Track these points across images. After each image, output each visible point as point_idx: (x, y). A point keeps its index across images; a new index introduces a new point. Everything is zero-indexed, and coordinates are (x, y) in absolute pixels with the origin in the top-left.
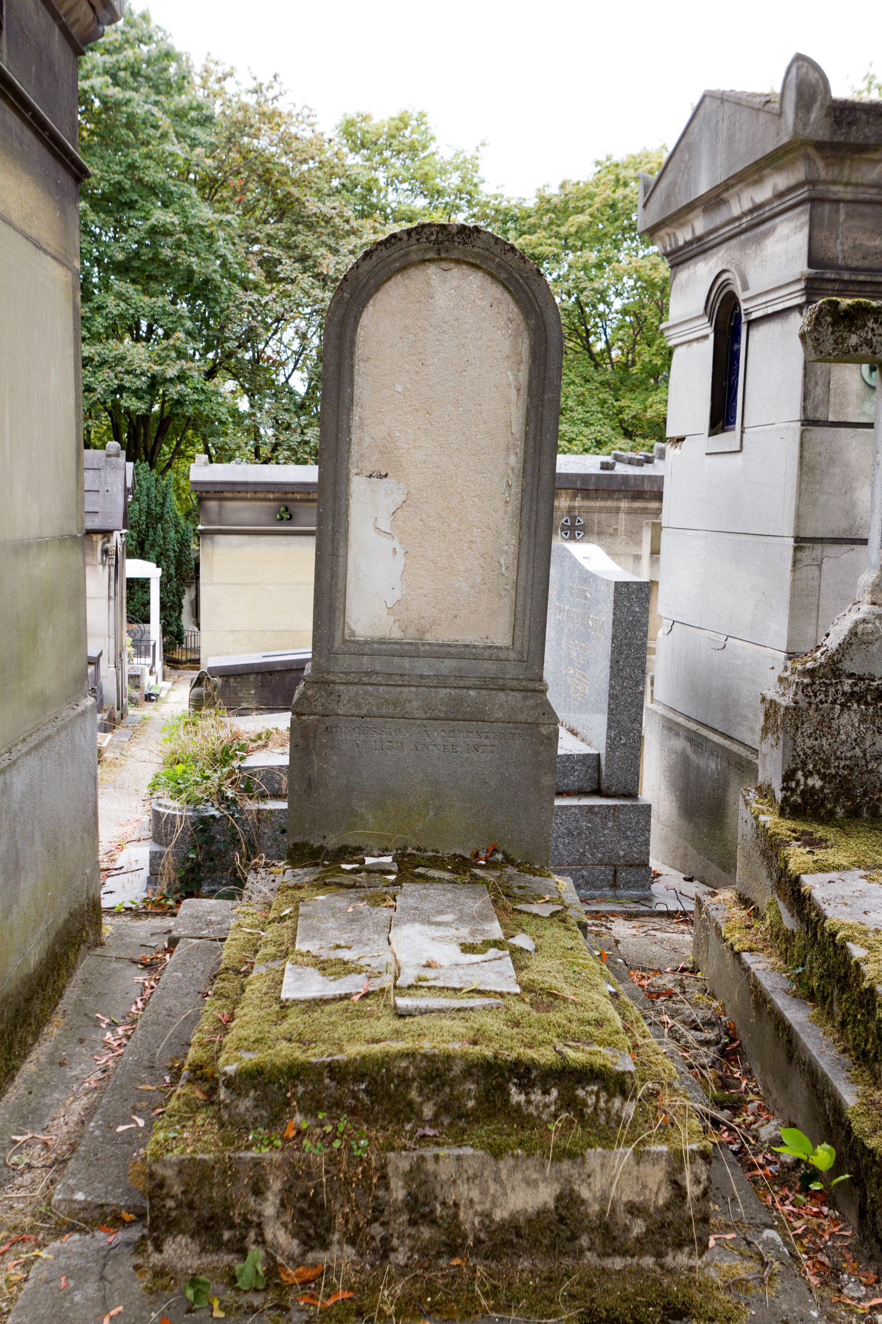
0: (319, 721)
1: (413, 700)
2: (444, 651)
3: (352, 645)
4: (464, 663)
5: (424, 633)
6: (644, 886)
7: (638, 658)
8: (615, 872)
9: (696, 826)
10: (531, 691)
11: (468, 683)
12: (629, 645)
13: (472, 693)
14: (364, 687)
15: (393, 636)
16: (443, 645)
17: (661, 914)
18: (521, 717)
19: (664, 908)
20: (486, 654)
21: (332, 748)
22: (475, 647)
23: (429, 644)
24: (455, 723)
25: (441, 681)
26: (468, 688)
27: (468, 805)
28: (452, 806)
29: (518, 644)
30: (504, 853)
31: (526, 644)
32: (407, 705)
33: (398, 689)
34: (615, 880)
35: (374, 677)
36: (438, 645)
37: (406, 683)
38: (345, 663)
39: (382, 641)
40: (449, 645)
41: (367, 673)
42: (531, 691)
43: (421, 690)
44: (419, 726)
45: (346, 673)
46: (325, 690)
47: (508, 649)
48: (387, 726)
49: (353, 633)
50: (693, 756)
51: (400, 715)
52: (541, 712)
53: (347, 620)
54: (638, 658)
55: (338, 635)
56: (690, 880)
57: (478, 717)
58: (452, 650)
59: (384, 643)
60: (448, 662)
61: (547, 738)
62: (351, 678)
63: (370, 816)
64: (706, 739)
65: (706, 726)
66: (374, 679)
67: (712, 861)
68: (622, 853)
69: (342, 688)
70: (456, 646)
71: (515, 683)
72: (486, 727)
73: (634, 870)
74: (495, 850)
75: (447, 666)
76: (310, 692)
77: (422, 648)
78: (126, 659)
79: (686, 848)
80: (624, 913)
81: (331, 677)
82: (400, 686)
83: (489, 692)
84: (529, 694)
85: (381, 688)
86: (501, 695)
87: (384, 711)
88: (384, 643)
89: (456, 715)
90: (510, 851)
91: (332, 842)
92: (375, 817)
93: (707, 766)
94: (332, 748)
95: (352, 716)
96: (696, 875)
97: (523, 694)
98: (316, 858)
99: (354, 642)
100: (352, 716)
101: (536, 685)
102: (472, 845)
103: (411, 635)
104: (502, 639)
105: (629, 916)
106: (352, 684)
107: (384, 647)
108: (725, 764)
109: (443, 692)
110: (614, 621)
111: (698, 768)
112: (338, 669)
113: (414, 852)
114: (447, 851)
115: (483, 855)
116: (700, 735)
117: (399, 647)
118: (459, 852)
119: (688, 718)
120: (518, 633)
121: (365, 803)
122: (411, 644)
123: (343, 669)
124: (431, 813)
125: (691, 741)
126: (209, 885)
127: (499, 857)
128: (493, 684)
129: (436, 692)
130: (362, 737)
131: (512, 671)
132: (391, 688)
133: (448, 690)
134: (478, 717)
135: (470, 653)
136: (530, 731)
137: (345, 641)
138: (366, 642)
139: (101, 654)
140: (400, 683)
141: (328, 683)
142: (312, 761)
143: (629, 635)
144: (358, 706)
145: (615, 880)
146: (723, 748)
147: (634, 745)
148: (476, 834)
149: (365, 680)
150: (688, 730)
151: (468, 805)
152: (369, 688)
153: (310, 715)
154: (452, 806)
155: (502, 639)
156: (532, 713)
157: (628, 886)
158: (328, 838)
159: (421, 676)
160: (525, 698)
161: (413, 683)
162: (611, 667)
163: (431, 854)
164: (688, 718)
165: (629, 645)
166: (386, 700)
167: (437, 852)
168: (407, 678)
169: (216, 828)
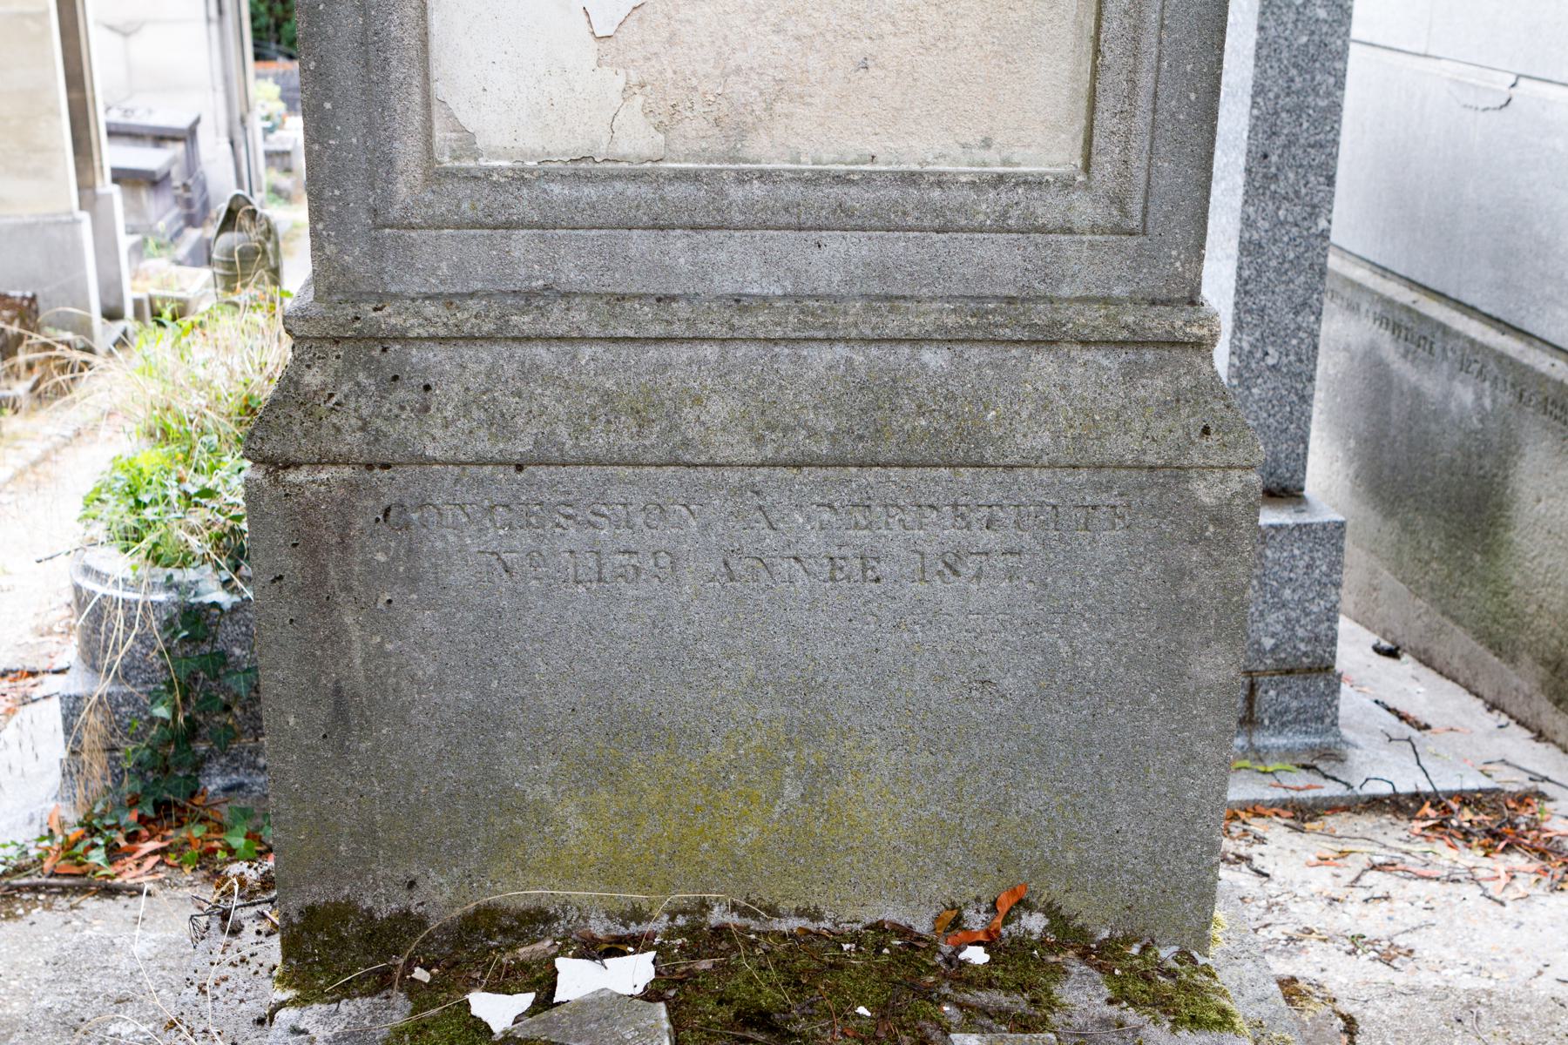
0: (352, 486)
1: (711, 393)
2: (825, 202)
3: (464, 190)
4: (898, 246)
5: (743, 131)
6: (1321, 719)
7: (1319, 145)
8: (1252, 688)
9: (1406, 527)
10: (1158, 344)
11: (917, 323)
12: (1298, 111)
13: (934, 358)
14: (520, 351)
15: (624, 147)
16: (816, 179)
17: (1374, 804)
18: (1122, 446)
19: (1385, 789)
20: (987, 206)
21: (413, 581)
22: (940, 181)
23: (764, 176)
24: (870, 475)
25: (812, 317)
26: (915, 341)
27: (924, 759)
28: (867, 766)
29: (1105, 167)
30: (1051, 911)
31: (1138, 164)
32: (689, 413)
33: (653, 353)
34: (1250, 707)
35: (557, 310)
36: (798, 177)
37: (678, 330)
38: (441, 259)
39: (581, 171)
40: (841, 179)
41: (529, 295)
42: (1158, 344)
43: (741, 351)
44: (738, 491)
45: (449, 300)
46: (370, 365)
47: (1067, 184)
48: (614, 494)
49: (467, 143)
50: (1405, 370)
51: (661, 453)
52: (1196, 423)
53: (439, 89)
54: (1319, 145)
55: (407, 152)
56: (1392, 653)
57: (961, 449)
58: (854, 196)
59: (590, 178)
60: (837, 244)
61: (1216, 520)
62: (467, 317)
63: (568, 811)
64: (1445, 329)
65: (1440, 296)
66: (557, 320)
67: (1457, 620)
68: (1268, 643)
69: (436, 356)
70: (868, 178)
71: (1093, 317)
72: (987, 485)
73: (1297, 682)
74: (1024, 904)
75: (834, 259)
76: (313, 379)
77: (736, 193)
78: (257, 125)
79: (1374, 573)
80: (1284, 805)
81: (391, 318)
82: (658, 340)
83: (998, 353)
84: (1149, 355)
85: (586, 352)
86: (1043, 360)
87: (599, 441)
88: (590, 178)
89: (873, 445)
90: (1071, 904)
91: (442, 898)
92: (586, 810)
93: (1447, 396)
94: (413, 581)
95: (481, 462)
96: (1407, 641)
97: (1125, 355)
98: (385, 953)
99: (471, 177)
100: (481, 462)
101: (1178, 320)
102: (940, 889)
103: (694, 143)
104: (1042, 143)
105: (1302, 814)
106: (471, 339)
107: (590, 192)
108: (1506, 398)
109: (822, 357)
110: (1259, 46)
111: (1417, 393)
112: (415, 285)
113: (733, 919)
114: (849, 913)
115: (976, 920)
116: (1423, 318)
117: (646, 191)
118: (892, 913)
119: (1385, 272)
120: (1105, 120)
121: (549, 765)
122: (695, 177)
123: (434, 285)
124: (791, 791)
125: (1382, 320)
126: (224, 772)
127: (1035, 923)
128: (1013, 323)
129: (797, 360)
130: (524, 539)
131: (1083, 269)
132: (625, 351)
133: (841, 350)
134: (961, 449)
135: (921, 205)
136: (1151, 496)
137: (437, 176)
138: (520, 178)
139: (197, 121)
140: (657, 330)
141: (383, 342)
142: (337, 635)
143: (1297, 85)
144: (501, 425)
145: (1250, 707)
146: (1501, 357)
147: (1297, 367)
148: (955, 855)
149: (523, 322)
150: (1389, 302)
151: (924, 759)
152: (541, 352)
153: (319, 463)
154: (867, 766)
155: (1042, 143)
156: (1159, 428)
157: (1282, 721)
158: (425, 887)
159: (738, 301)
160: (1131, 374)
161: (704, 328)
162: (1248, 171)
163: (792, 924)
164: (1385, 272)
165: (1298, 111)
166: (607, 398)
167: (816, 916)
168: (682, 308)
169: (227, 631)
